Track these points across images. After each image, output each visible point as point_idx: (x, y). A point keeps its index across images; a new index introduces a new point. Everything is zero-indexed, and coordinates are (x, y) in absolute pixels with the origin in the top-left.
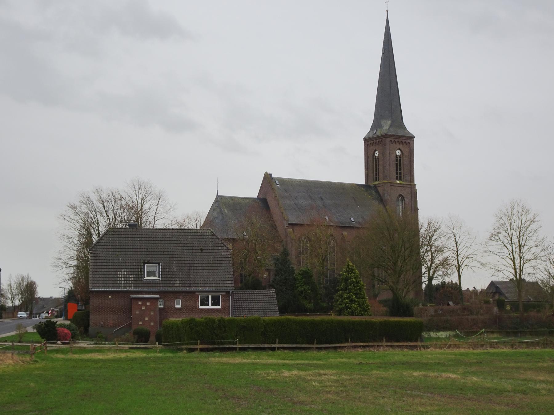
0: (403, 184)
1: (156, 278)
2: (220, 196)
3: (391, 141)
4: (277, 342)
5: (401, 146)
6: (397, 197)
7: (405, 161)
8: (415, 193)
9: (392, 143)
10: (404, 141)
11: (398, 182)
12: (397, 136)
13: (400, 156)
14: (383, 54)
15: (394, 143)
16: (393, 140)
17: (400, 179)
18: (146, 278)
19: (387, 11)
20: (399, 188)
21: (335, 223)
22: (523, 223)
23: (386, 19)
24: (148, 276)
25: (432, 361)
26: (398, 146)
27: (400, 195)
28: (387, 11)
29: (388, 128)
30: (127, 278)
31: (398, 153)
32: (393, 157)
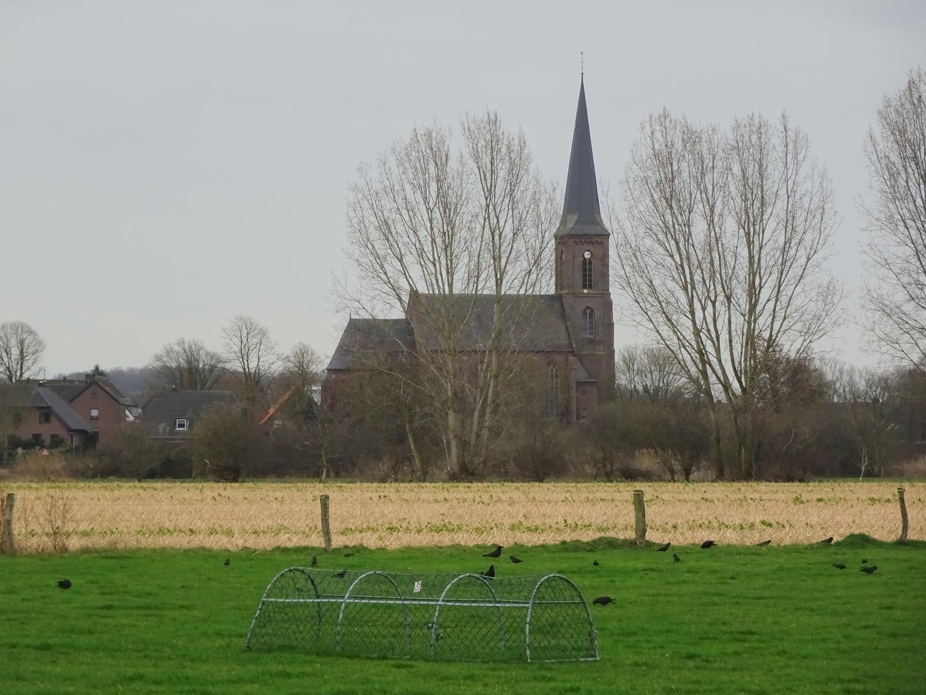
0: (593, 294)
1: (185, 429)
2: (353, 319)
3: (575, 241)
4: (882, 475)
5: (590, 247)
6: (583, 309)
7: (596, 265)
8: (610, 304)
9: (577, 244)
10: (594, 241)
11: (585, 291)
12: (584, 235)
13: (590, 259)
14: (575, 129)
15: (580, 244)
16: (578, 240)
17: (590, 287)
18: (178, 429)
19: (582, 74)
20: (586, 298)
21: (831, 288)
22: (781, 330)
23: (580, 90)
24: (179, 427)
25: (252, 510)
26: (586, 246)
27: (588, 308)
28: (582, 74)
29: (572, 225)
30: (164, 429)
31: (587, 255)
32: (579, 260)
